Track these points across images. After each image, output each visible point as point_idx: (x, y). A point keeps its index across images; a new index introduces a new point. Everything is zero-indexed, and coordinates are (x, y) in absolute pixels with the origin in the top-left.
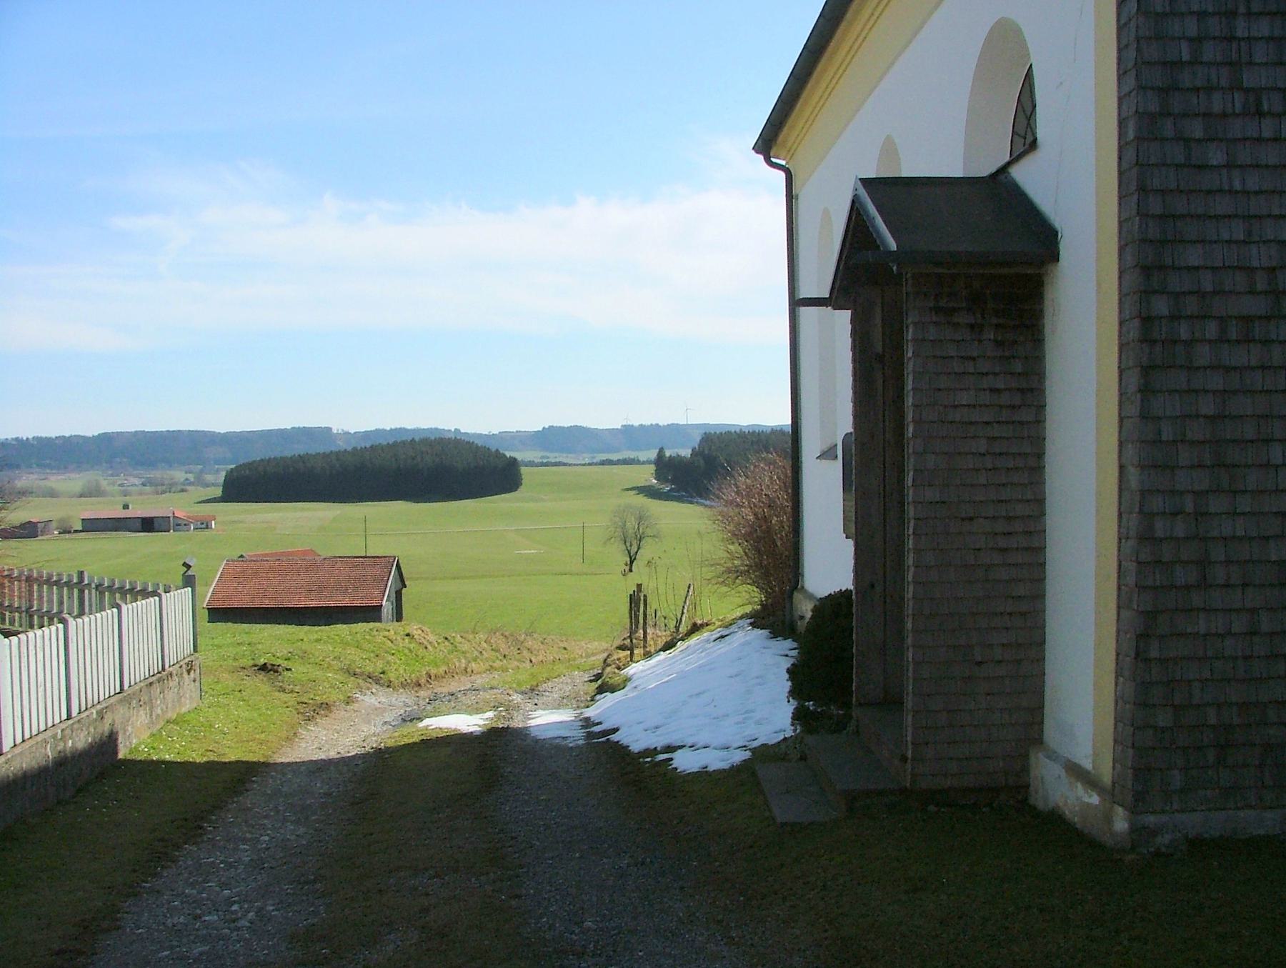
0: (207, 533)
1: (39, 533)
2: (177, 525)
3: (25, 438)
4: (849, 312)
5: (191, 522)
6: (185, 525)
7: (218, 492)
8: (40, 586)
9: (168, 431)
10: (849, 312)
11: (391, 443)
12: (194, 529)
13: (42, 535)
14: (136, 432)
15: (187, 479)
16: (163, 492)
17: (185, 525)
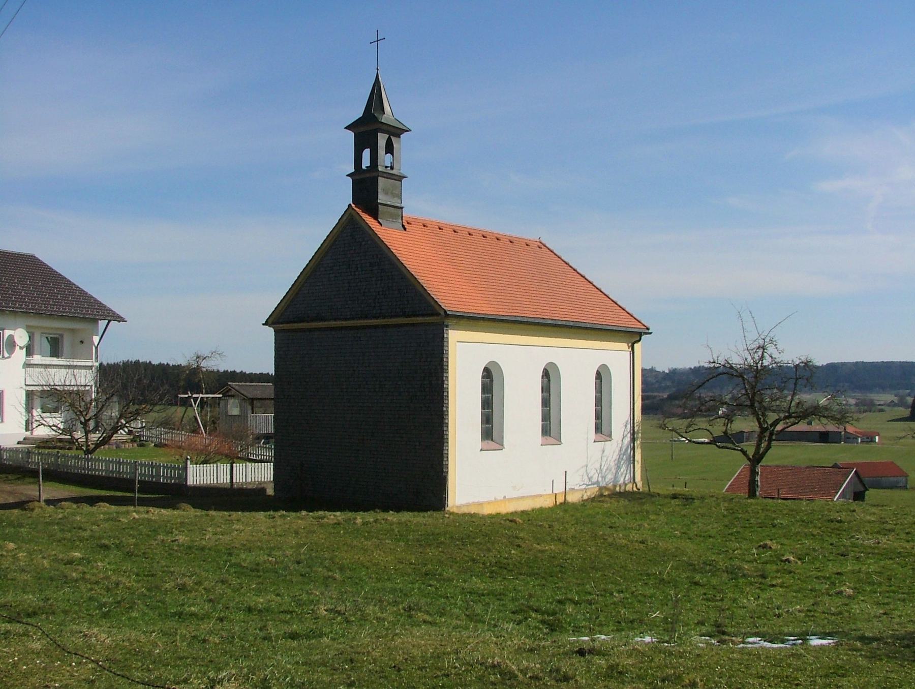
0: (873, 445)
1: (745, 440)
2: (848, 438)
3: (166, 364)
4: (369, 149)
5: (859, 437)
6: (854, 438)
7: (907, 412)
8: (35, 456)
9: (883, 362)
10: (369, 149)
11: (141, 361)
12: (861, 442)
13: (746, 442)
14: (857, 363)
15: (893, 401)
16: (865, 411)
17: (854, 438)
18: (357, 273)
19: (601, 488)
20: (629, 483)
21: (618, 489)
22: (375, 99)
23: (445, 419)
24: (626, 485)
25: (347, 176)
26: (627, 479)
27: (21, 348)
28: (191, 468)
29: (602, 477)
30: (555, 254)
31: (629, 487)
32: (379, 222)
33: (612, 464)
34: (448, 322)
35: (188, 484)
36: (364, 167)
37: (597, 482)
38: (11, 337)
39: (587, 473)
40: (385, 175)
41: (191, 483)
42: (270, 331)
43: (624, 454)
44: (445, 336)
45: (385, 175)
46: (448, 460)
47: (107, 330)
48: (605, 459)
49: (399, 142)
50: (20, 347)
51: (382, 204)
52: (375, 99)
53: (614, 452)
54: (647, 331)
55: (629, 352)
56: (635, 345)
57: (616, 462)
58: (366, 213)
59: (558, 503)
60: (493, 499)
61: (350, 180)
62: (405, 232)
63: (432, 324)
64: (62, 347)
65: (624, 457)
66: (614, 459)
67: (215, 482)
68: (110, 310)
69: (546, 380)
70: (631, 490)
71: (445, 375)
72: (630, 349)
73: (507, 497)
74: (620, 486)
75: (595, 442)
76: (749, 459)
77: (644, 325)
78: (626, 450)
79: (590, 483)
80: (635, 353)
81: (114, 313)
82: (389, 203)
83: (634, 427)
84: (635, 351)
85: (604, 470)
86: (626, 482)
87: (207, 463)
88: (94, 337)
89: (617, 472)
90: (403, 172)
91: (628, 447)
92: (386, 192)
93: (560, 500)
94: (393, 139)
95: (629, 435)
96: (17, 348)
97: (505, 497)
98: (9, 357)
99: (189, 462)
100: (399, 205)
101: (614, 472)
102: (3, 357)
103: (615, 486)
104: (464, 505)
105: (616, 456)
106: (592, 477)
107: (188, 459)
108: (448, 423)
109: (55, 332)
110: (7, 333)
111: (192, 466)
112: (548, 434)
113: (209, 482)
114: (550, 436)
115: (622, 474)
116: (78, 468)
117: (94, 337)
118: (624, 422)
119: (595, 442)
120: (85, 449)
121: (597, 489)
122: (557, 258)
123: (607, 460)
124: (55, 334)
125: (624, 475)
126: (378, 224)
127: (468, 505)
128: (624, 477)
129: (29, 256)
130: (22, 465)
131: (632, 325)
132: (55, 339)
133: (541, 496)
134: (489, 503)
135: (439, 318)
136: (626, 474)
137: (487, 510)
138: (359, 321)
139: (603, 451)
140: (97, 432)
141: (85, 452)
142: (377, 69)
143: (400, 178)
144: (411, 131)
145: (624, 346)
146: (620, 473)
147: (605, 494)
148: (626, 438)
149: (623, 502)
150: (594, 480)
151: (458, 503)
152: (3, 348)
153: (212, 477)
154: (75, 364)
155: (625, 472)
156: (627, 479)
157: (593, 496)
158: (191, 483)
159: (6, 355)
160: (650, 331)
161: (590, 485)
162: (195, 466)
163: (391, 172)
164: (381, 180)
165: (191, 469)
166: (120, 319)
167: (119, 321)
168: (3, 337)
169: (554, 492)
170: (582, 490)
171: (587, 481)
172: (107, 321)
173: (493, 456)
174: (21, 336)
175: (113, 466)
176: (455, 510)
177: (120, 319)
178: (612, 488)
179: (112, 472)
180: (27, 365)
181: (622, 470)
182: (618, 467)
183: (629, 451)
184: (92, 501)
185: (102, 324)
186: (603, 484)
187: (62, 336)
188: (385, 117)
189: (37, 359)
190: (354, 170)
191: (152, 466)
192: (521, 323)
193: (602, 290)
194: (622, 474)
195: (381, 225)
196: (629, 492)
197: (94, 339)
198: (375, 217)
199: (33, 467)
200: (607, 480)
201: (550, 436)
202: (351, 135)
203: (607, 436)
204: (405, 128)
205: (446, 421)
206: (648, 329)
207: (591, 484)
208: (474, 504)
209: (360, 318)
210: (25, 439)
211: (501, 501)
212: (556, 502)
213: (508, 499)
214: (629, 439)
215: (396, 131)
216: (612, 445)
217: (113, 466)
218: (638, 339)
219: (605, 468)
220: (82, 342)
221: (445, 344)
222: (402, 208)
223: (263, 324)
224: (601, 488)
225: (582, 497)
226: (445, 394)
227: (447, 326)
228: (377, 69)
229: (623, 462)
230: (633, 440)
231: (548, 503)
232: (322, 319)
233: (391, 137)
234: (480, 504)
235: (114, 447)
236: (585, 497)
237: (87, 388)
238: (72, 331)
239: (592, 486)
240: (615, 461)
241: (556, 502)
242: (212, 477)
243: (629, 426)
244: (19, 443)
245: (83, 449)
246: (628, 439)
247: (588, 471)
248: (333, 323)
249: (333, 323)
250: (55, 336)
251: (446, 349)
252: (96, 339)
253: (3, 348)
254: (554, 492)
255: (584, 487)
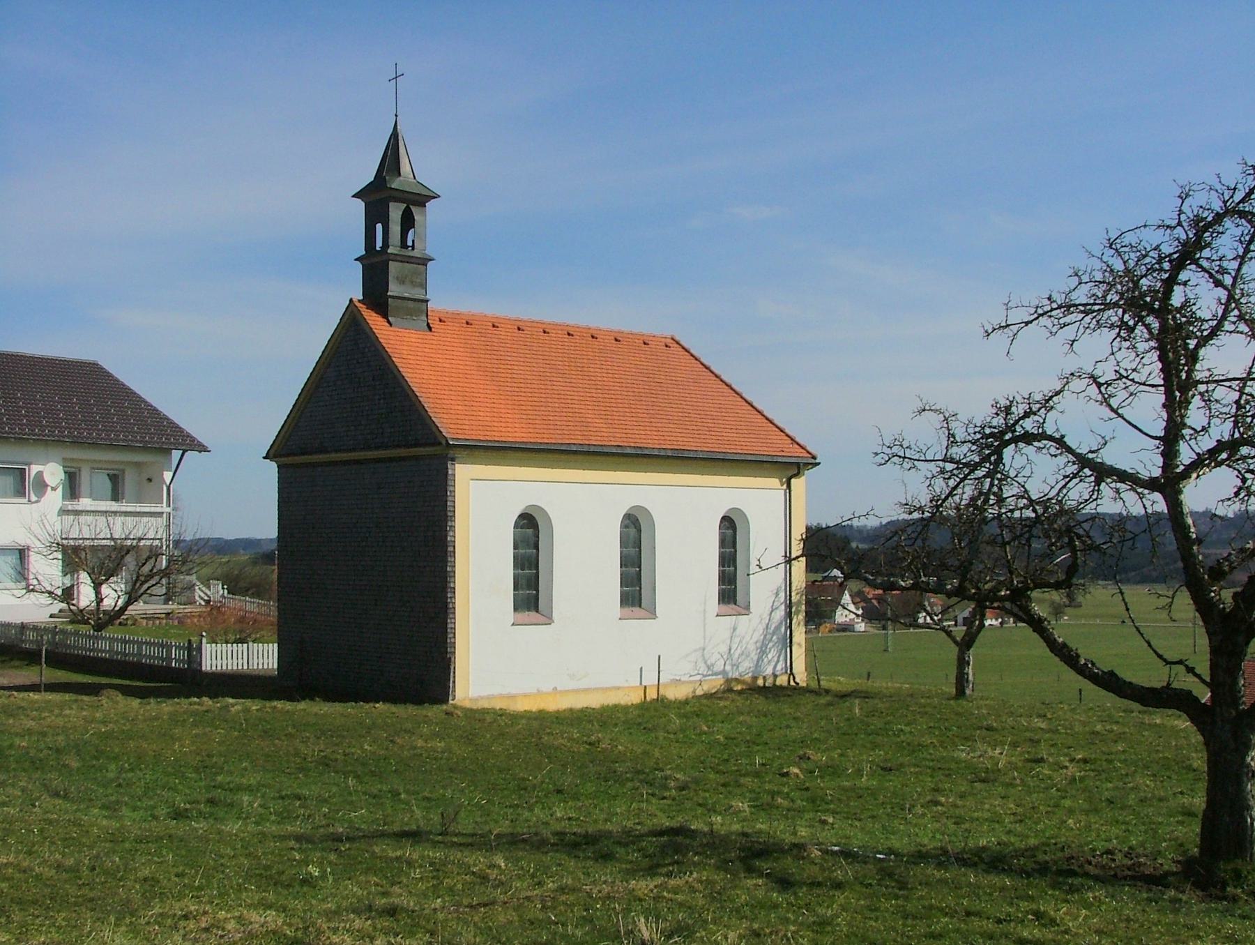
18: (359, 390)
19: (728, 681)
20: (782, 674)
21: (760, 682)
22: (391, 160)
23: (450, 582)
24: (775, 676)
25: (356, 260)
26: (779, 667)
27: (54, 489)
28: (207, 648)
29: (733, 666)
30: (692, 355)
31: (782, 680)
32: (389, 322)
33: (752, 647)
34: (451, 453)
35: (204, 669)
36: (378, 249)
37: (724, 672)
38: (40, 475)
39: (704, 659)
40: (399, 258)
41: (209, 668)
42: (272, 467)
43: (774, 633)
44: (450, 472)
45: (399, 258)
46: (455, 637)
47: (180, 466)
48: (737, 640)
49: (424, 214)
50: (52, 488)
51: (393, 297)
52: (391, 160)
53: (754, 631)
54: (813, 461)
55: (783, 491)
56: (793, 480)
57: (759, 645)
58: (372, 310)
59: (648, 699)
60: (535, 691)
61: (359, 265)
62: (429, 333)
63: (431, 457)
64: (79, 486)
65: (775, 637)
66: (755, 639)
67: (245, 667)
68: (189, 436)
69: (632, 531)
70: (785, 684)
71: (449, 524)
72: (785, 487)
73: (558, 689)
74: (764, 678)
75: (717, 615)
76: (955, 642)
77: (808, 452)
78: (777, 628)
79: (710, 672)
80: (792, 493)
81: (193, 439)
82: (406, 295)
83: (790, 596)
84: (792, 488)
85: (736, 656)
86: (778, 673)
87: (242, 643)
88: (165, 473)
89: (760, 659)
90: (430, 252)
91: (781, 623)
92: (401, 281)
93: (652, 695)
94: (413, 209)
95: (783, 607)
96: (49, 488)
97: (555, 689)
98: (37, 502)
99: (204, 640)
100: (422, 297)
101: (755, 658)
102: (29, 501)
103: (755, 678)
104: (482, 698)
105: (758, 636)
106: (713, 665)
107: (203, 636)
108: (454, 588)
109: (116, 467)
110: (35, 469)
111: (209, 645)
112: (637, 601)
113: (230, 668)
114: (640, 606)
115: (769, 662)
116: (154, 657)
117: (165, 473)
118: (774, 588)
119: (717, 615)
120: (93, 623)
121: (722, 681)
122: (694, 361)
123: (741, 641)
124: (71, 467)
125: (773, 664)
126: (387, 324)
127: (490, 698)
128: (772, 668)
129: (72, 362)
130: (15, 643)
131: (794, 453)
132: (115, 475)
133: (619, 688)
134: (526, 696)
135: (438, 448)
136: (778, 661)
137: (521, 706)
138: (362, 453)
139: (735, 629)
140: (170, 603)
141: (93, 626)
142: (396, 116)
143: (424, 261)
144: (439, 196)
145: (775, 482)
146: (766, 660)
147: (735, 689)
148: (778, 611)
149: (760, 702)
150: (719, 667)
151: (474, 692)
152: (29, 487)
153: (240, 660)
154: (138, 509)
155: (776, 659)
156: (779, 667)
157: (713, 691)
158: (209, 668)
159: (34, 498)
160: (817, 461)
161: (709, 675)
162: (224, 645)
163: (411, 254)
164: (394, 267)
165: (209, 650)
166: (202, 448)
167: (200, 452)
168: (29, 478)
169: (644, 684)
170: (695, 682)
171: (703, 670)
172: (181, 451)
173: (534, 634)
174: (53, 473)
175: (118, 646)
176: (468, 704)
177: (202, 448)
178: (749, 680)
179: (117, 653)
180: (64, 512)
181: (770, 656)
182: (763, 651)
183: (783, 629)
184: (93, 690)
185: (176, 454)
186: (734, 674)
187: (123, 471)
188: (400, 181)
189: (85, 503)
190: (364, 253)
191: (162, 646)
192: (588, 453)
193: (755, 404)
194: (769, 662)
195: (391, 325)
196: (781, 687)
197: (165, 476)
198: (385, 315)
199: (27, 646)
200: (741, 669)
201: (640, 606)
202: (360, 205)
203: (744, 609)
204: (432, 194)
205: (452, 585)
206: (814, 458)
207: (712, 675)
208: (501, 697)
209: (362, 450)
210: (60, 611)
211: (548, 693)
212: (645, 697)
213: (561, 691)
214: (783, 613)
215: (421, 199)
216: (750, 621)
217: (118, 646)
218: (796, 472)
219: (739, 651)
220: (150, 480)
221: (450, 483)
222: (427, 301)
223: (264, 458)
224: (728, 681)
225: (694, 692)
226: (450, 549)
227: (453, 459)
228: (396, 116)
229: (771, 644)
230: (789, 615)
231: (635, 698)
232: (325, 451)
233: (411, 207)
234: (512, 697)
235: (176, 622)
236: (699, 692)
237: (157, 543)
238: (138, 465)
239: (714, 677)
240: (756, 643)
241: (645, 697)
242: (240, 660)
243: (782, 595)
244: (51, 616)
245: (90, 624)
246: (780, 613)
247: (707, 657)
248: (334, 456)
249: (334, 456)
250: (115, 472)
251: (452, 489)
252: (168, 476)
253: (29, 487)
254: (644, 684)
255: (698, 678)
